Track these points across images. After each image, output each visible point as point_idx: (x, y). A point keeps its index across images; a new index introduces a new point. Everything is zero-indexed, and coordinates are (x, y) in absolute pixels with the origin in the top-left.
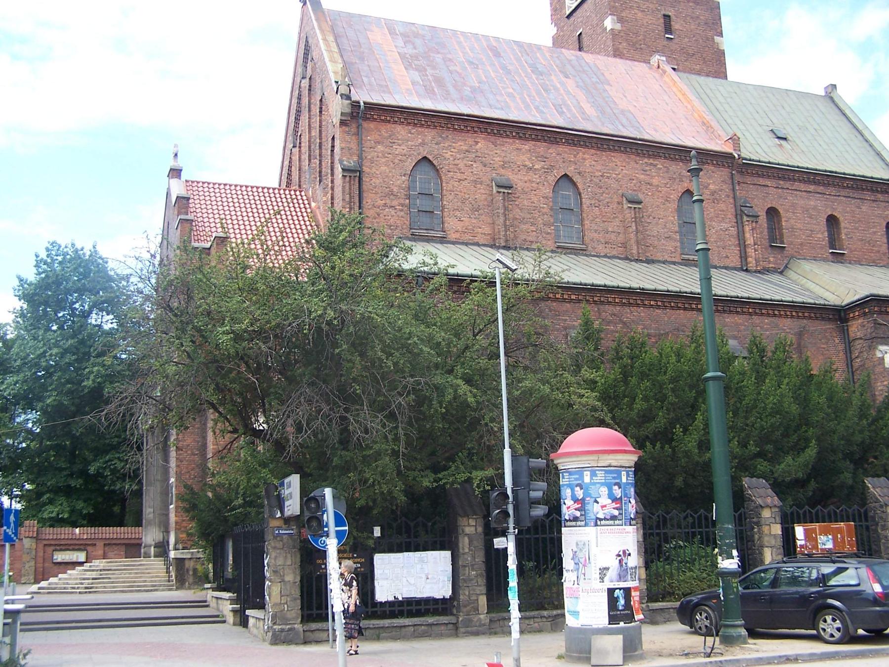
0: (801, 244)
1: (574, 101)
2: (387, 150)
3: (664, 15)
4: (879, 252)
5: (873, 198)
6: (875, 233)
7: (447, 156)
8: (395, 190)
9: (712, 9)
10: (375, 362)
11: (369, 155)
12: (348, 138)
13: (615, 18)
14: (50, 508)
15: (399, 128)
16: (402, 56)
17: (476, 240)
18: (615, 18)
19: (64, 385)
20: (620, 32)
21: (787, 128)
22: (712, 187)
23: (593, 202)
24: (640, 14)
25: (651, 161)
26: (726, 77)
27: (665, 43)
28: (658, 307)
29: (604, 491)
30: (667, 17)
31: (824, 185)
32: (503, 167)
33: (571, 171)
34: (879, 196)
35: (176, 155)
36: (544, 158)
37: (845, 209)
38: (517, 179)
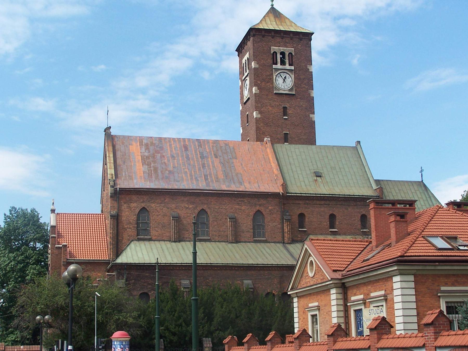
0: (315, 228)
1: (215, 172)
3: (284, 107)
5: (355, 204)
6: (354, 220)
7: (152, 206)
8: (131, 221)
12: (113, 202)
13: (258, 112)
14: (12, 336)
15: (134, 196)
16: (143, 157)
18: (258, 112)
19: (17, 279)
20: (260, 118)
21: (325, 169)
22: (270, 208)
24: (271, 109)
25: (242, 199)
26: (310, 139)
27: (283, 121)
28: (219, 270)
29: (119, 346)
30: (285, 108)
31: (329, 200)
32: (176, 208)
34: (358, 203)
35: (53, 203)
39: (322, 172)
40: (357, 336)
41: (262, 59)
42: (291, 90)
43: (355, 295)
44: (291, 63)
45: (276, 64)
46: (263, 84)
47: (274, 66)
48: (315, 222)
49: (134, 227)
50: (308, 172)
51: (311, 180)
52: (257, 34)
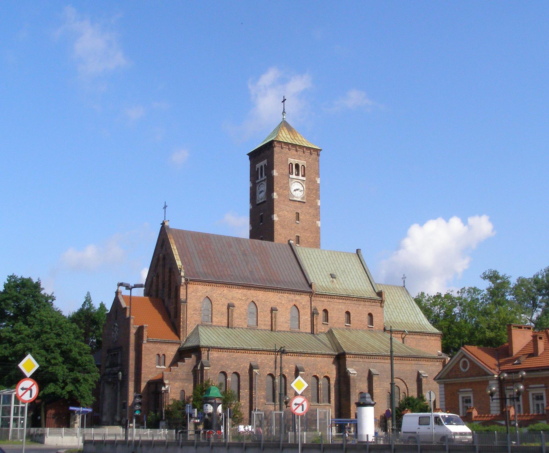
9: (316, 209)
22: (303, 303)
24: (286, 213)
32: (232, 299)
33: (254, 300)
34: (366, 303)
36: (245, 295)
38: (236, 303)
39: (335, 274)
40: (524, 413)
42: (303, 198)
45: (292, 174)
46: (281, 190)
47: (291, 176)
50: (326, 274)
51: (328, 280)
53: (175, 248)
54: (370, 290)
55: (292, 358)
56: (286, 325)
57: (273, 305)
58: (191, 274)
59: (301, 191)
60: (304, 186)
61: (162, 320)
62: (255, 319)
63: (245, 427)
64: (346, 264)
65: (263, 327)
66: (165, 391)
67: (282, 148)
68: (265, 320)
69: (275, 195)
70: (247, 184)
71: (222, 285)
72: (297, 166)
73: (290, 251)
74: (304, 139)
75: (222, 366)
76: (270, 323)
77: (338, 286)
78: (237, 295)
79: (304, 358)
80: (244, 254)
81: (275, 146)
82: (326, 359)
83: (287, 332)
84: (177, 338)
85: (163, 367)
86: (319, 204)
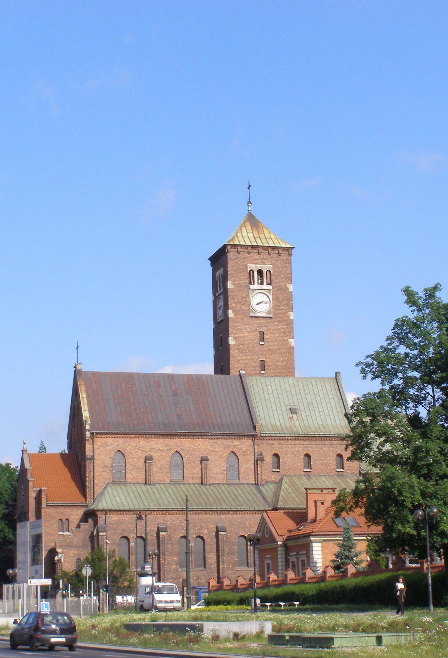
0: (289, 469)
2: (104, 449)
3: (260, 332)
4: (330, 468)
5: (330, 443)
6: (329, 460)
7: (128, 449)
8: (107, 464)
10: (196, 524)
11: (96, 452)
17: (138, 481)
21: (301, 405)
22: (244, 449)
23: (188, 461)
24: (246, 334)
25: (216, 441)
26: (288, 370)
27: (260, 347)
32: (150, 451)
33: (179, 449)
34: (334, 442)
37: (313, 449)
38: (155, 455)
39: (297, 407)
41: (238, 278)
42: (269, 312)
43: (292, 552)
44: (269, 282)
45: (254, 284)
47: (251, 286)
48: (289, 462)
49: (110, 470)
50: (284, 409)
51: (286, 417)
52: (233, 250)
53: (84, 396)
54: (343, 424)
55: (211, 517)
56: (222, 476)
57: (204, 454)
58: (100, 425)
59: (266, 302)
60: (271, 297)
61: (70, 479)
62: (181, 472)
63: (123, 598)
64: (316, 393)
65: (191, 481)
66: (58, 560)
67: (238, 253)
68: (193, 471)
69: (230, 313)
70: (210, 298)
71: (136, 436)
72: (260, 272)
73: (239, 384)
74: (272, 236)
75: (124, 530)
76: (200, 475)
77: (297, 424)
78: (157, 446)
79: (227, 516)
80: (175, 394)
81: (228, 252)
82: (249, 515)
83: (223, 484)
84: (83, 499)
85: (67, 533)
86: (292, 317)
